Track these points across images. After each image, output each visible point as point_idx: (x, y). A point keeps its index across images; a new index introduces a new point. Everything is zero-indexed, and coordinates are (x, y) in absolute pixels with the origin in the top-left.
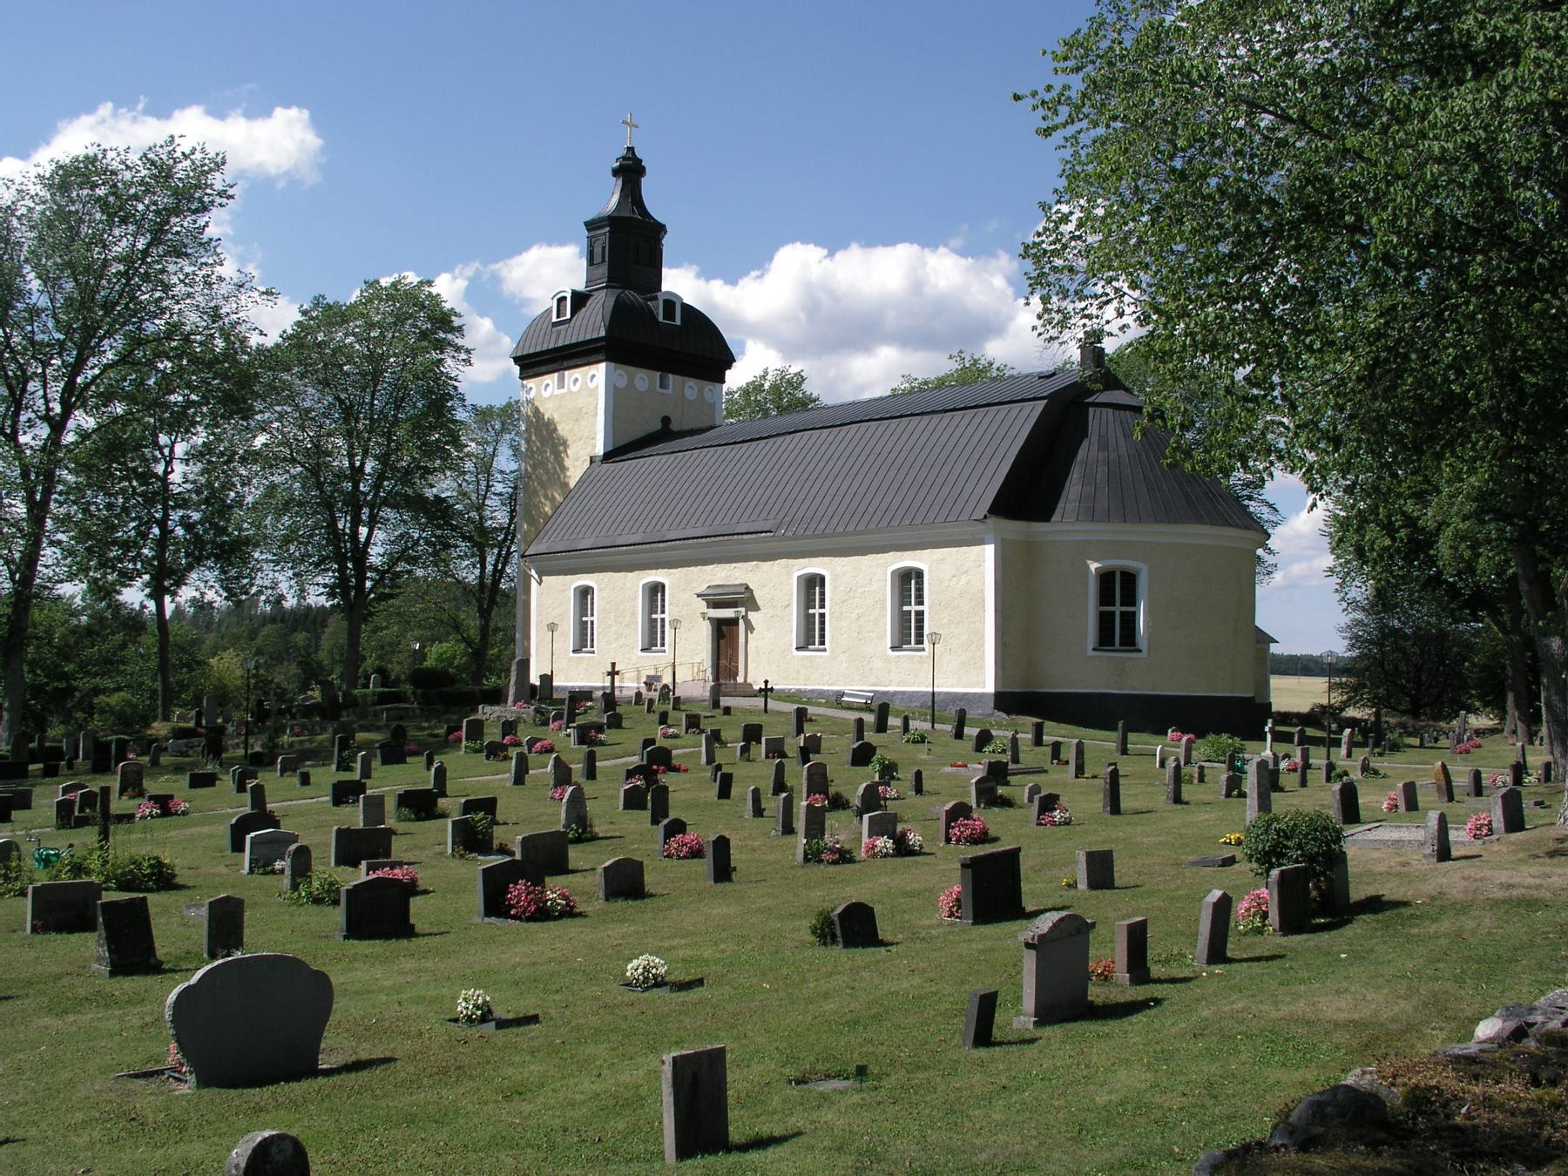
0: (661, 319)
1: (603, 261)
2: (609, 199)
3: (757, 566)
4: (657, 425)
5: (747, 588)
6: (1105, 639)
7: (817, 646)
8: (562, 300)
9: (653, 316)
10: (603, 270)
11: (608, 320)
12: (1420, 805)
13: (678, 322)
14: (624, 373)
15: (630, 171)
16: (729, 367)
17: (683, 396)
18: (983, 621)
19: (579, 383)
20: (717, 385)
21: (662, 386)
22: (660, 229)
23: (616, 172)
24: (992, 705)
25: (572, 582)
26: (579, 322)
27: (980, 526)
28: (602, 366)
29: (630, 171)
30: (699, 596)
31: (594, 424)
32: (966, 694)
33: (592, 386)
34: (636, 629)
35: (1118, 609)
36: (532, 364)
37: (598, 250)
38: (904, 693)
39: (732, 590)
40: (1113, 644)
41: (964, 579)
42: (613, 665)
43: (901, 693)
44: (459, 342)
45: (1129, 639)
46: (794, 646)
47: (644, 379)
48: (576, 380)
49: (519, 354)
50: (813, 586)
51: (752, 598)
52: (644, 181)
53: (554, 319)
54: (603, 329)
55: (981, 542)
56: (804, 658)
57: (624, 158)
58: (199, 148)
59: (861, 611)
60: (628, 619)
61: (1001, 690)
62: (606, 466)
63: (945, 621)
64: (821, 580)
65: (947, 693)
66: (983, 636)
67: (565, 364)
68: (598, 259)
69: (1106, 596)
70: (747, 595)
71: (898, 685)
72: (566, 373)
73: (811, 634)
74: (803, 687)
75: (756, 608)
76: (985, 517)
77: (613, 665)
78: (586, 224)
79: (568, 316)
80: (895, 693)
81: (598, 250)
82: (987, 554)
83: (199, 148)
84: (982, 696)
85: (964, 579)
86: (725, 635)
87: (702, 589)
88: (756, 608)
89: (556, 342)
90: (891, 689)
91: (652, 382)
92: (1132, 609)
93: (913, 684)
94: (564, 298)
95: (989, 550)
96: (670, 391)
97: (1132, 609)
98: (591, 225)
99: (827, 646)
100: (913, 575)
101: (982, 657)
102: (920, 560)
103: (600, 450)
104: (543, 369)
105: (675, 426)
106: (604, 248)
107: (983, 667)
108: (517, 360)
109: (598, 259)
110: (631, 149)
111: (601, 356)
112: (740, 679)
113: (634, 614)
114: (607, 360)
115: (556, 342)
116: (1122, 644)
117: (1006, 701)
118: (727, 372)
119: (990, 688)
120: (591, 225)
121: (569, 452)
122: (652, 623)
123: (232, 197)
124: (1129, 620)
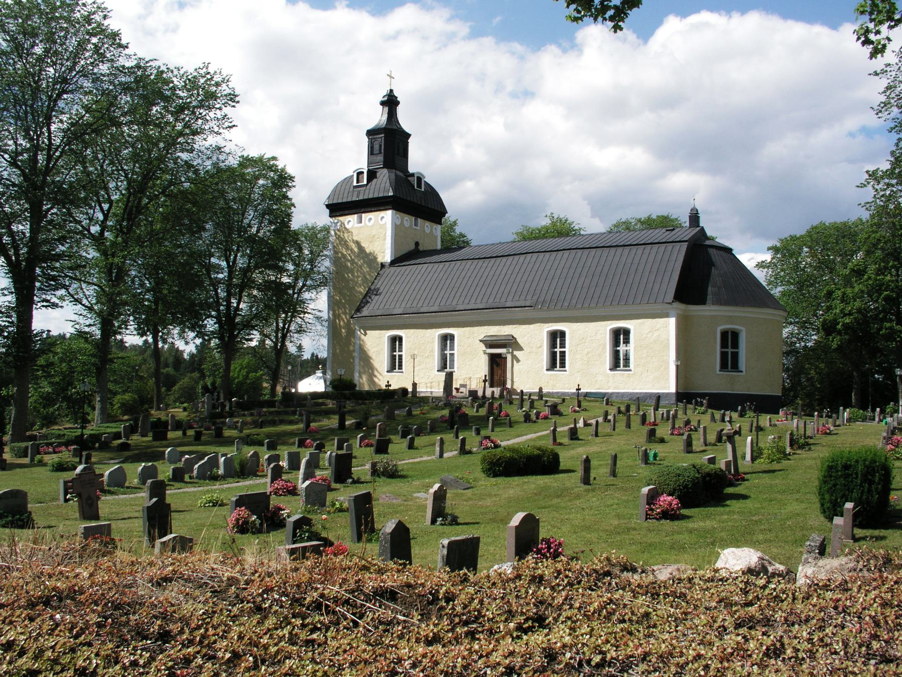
1: (380, 153)
2: (377, 117)
4: (412, 247)
5: (513, 337)
6: (724, 366)
7: (397, 370)
8: (360, 174)
10: (381, 158)
11: (393, 184)
12: (389, 451)
13: (423, 190)
14: (399, 215)
15: (391, 102)
19: (372, 222)
22: (408, 136)
23: (383, 103)
26: (373, 186)
29: (391, 102)
30: (481, 341)
35: (730, 350)
36: (337, 209)
37: (376, 147)
38: (618, 393)
39: (503, 338)
40: (619, 367)
41: (656, 334)
42: (388, 382)
43: (616, 393)
45: (735, 367)
46: (545, 368)
47: (408, 220)
48: (370, 219)
49: (331, 202)
50: (557, 338)
51: (516, 343)
53: (355, 184)
54: (391, 190)
55: (666, 315)
56: (551, 375)
58: (218, 72)
60: (427, 354)
62: (393, 269)
63: (645, 355)
64: (562, 334)
67: (362, 210)
68: (376, 150)
69: (724, 344)
71: (614, 389)
72: (363, 215)
73: (556, 361)
74: (551, 391)
75: (520, 349)
77: (388, 382)
79: (365, 182)
80: (612, 393)
81: (376, 147)
82: (672, 322)
83: (218, 72)
84: (668, 394)
85: (656, 334)
86: (497, 364)
87: (481, 337)
88: (520, 349)
89: (358, 196)
90: (610, 391)
91: (411, 222)
92: (736, 350)
93: (624, 388)
94: (362, 173)
97: (736, 350)
98: (370, 133)
99: (404, 370)
100: (622, 332)
101: (668, 373)
105: (421, 248)
106: (380, 146)
107: (668, 379)
108: (328, 206)
110: (391, 91)
111: (388, 207)
113: (432, 351)
114: (393, 209)
115: (358, 196)
116: (732, 368)
117: (684, 396)
119: (672, 389)
122: (393, 358)
123: (238, 102)
124: (735, 356)
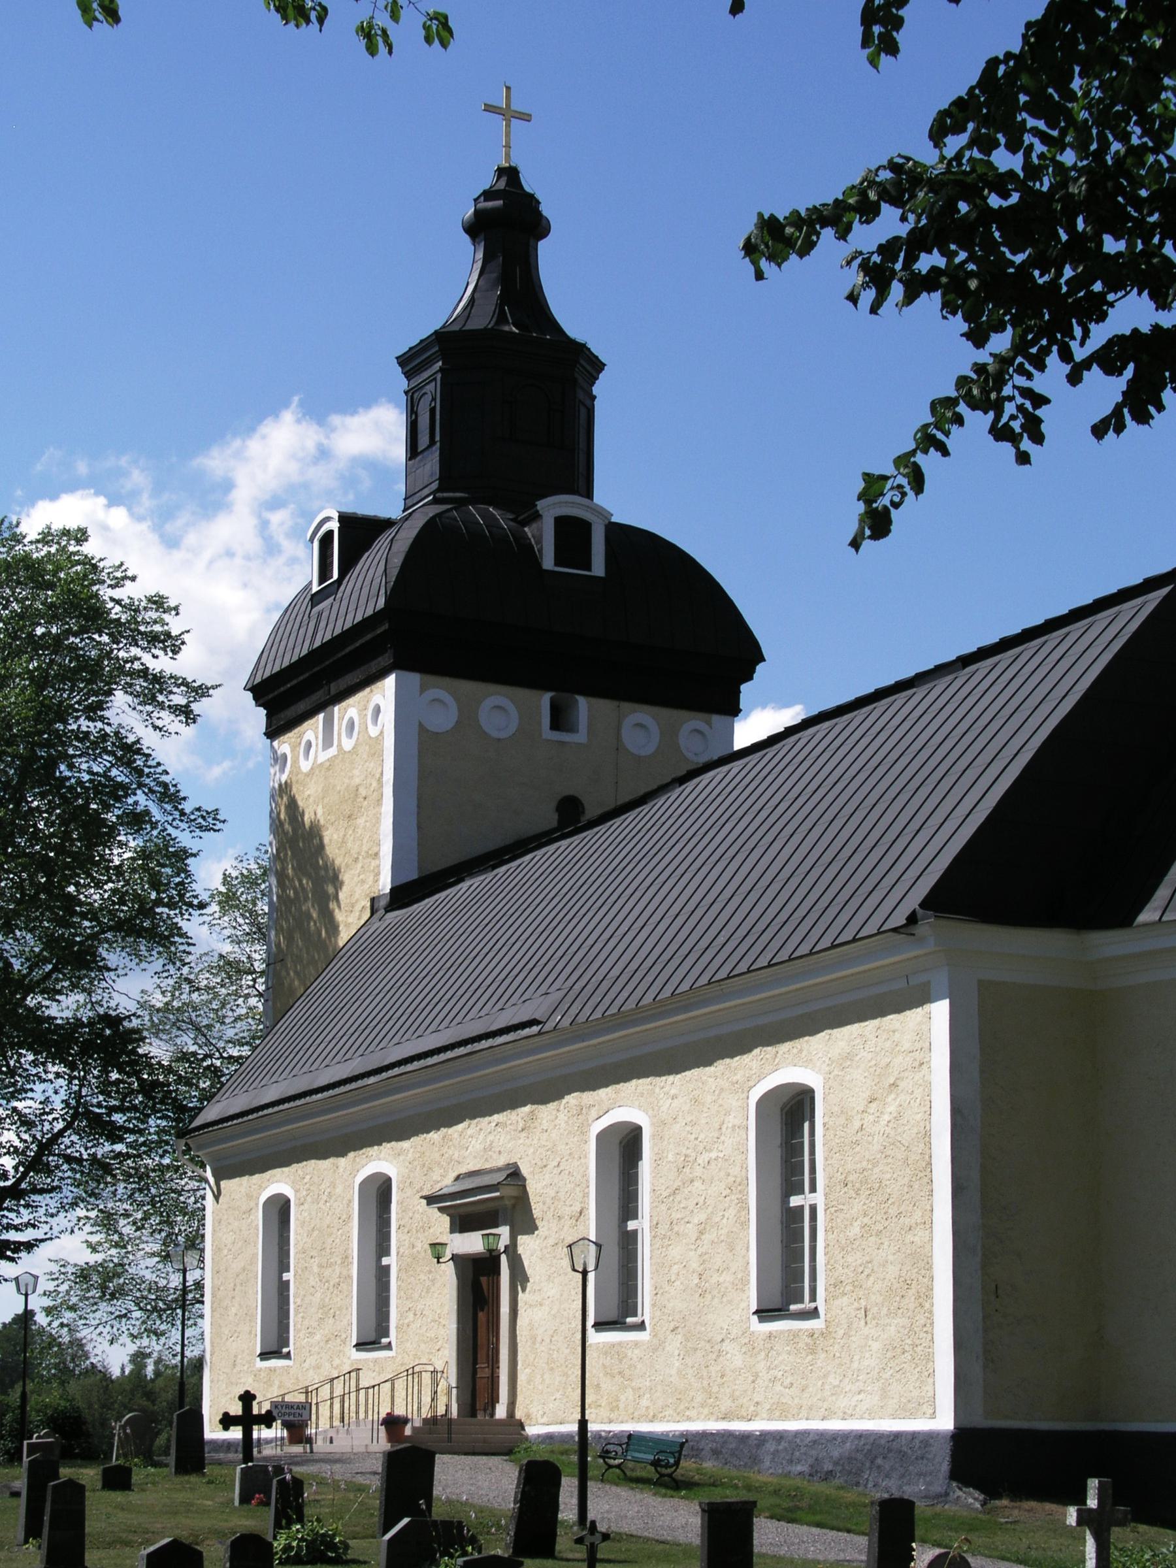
0: (548, 562)
1: (432, 442)
3: (532, 1116)
9: (530, 555)
13: (598, 568)
16: (749, 677)
17: (619, 747)
18: (928, 1224)
20: (716, 719)
21: (556, 725)
24: (945, 1467)
25: (262, 1188)
27: (907, 953)
28: (390, 682)
30: (431, 1200)
31: (378, 820)
32: (897, 1435)
33: (373, 731)
34: (349, 1295)
44: (159, 663)
51: (522, 1200)
52: (547, 251)
55: (920, 997)
57: (488, 195)
59: (702, 1217)
61: (980, 1421)
63: (856, 1230)
65: (860, 1436)
66: (929, 1266)
68: (423, 440)
70: (509, 1191)
76: (912, 919)
78: (403, 361)
79: (336, 576)
84: (925, 1440)
87: (444, 1182)
95: (940, 1010)
96: (580, 737)
102: (808, 1063)
103: (385, 884)
104: (302, 706)
107: (929, 1358)
109: (423, 440)
111: (385, 660)
112: (501, 1412)
113: (346, 1258)
114: (399, 664)
118: (744, 688)
119: (945, 1422)
120: (410, 362)
121: (341, 895)
